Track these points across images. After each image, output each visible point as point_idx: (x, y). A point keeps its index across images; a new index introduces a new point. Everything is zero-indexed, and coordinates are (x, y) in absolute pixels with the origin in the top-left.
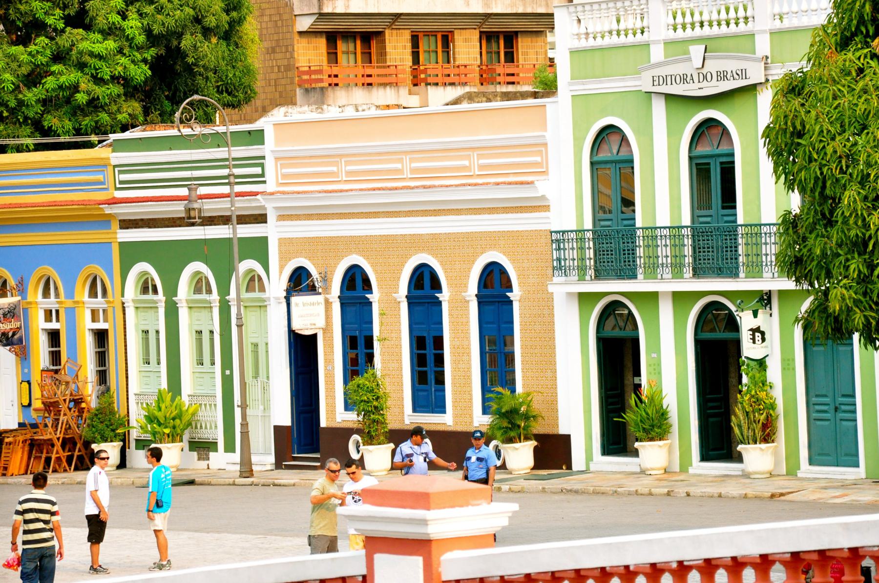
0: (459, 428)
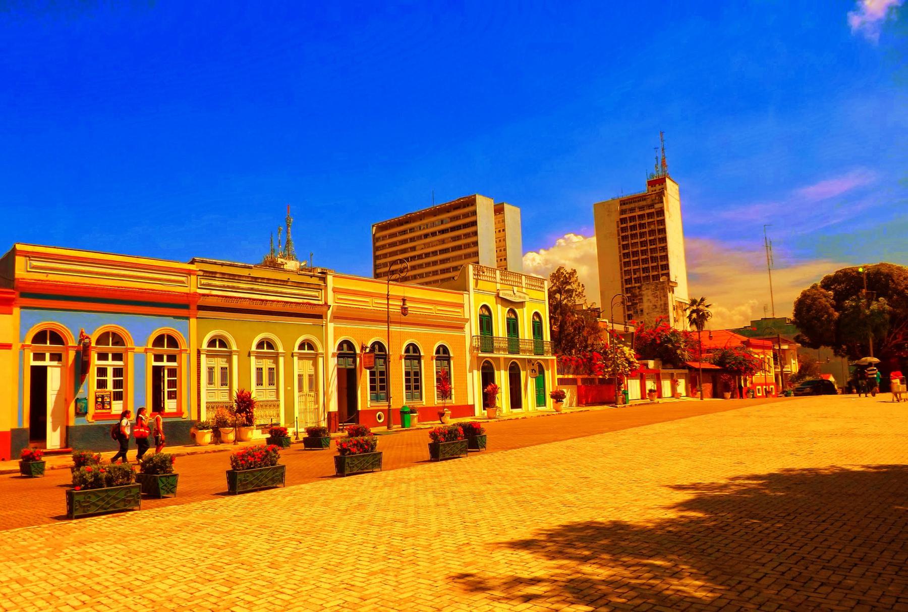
0: (460, 404)
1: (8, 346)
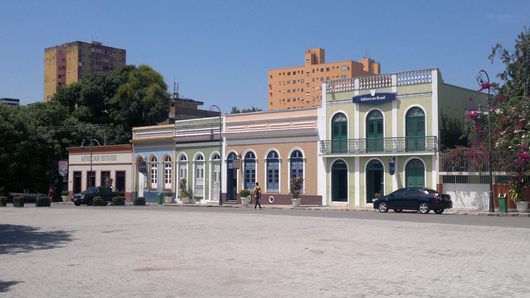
1: (131, 164)
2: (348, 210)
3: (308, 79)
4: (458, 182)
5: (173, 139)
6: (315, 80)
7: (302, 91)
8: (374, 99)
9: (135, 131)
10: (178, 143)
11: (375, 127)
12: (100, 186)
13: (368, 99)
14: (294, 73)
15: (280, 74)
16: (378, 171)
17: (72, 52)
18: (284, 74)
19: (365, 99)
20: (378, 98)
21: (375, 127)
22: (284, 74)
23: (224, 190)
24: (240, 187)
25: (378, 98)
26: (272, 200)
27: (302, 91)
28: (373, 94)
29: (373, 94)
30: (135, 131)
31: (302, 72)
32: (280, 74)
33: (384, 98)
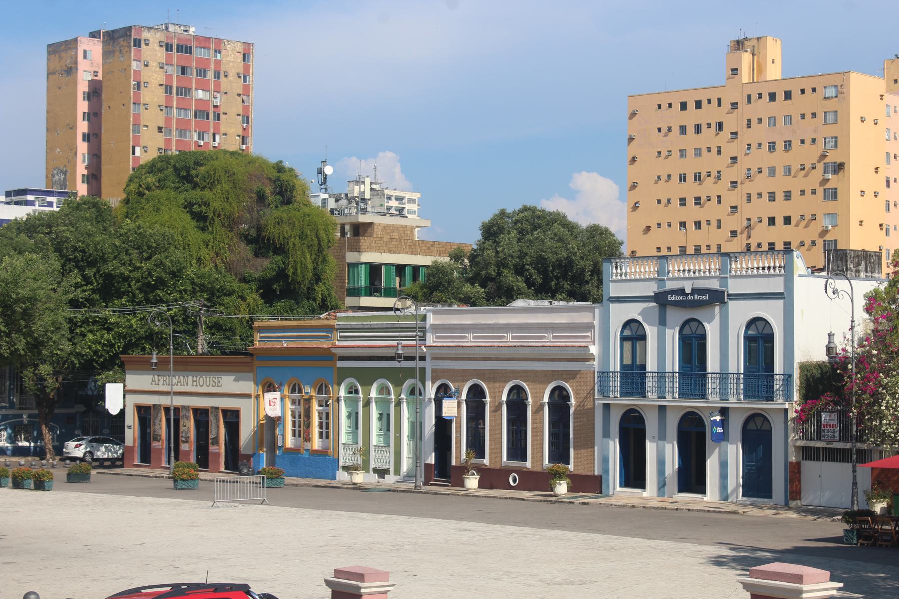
2: (633, 506)
3: (732, 123)
4: (826, 459)
5: (333, 351)
6: (754, 123)
7: (719, 153)
8: (690, 298)
9: (261, 330)
10: (343, 358)
11: (693, 347)
12: (86, 193)
13: (680, 298)
14: (698, 105)
15: (660, 106)
16: (492, 487)
17: (117, 53)
18: (670, 105)
19: (673, 298)
20: (696, 297)
21: (693, 347)
22: (670, 105)
23: (431, 460)
24: (460, 451)
25: (696, 297)
26: (515, 480)
27: (719, 153)
28: (688, 290)
29: (688, 290)
30: (261, 330)
31: (719, 100)
32: (660, 106)
33: (705, 298)
